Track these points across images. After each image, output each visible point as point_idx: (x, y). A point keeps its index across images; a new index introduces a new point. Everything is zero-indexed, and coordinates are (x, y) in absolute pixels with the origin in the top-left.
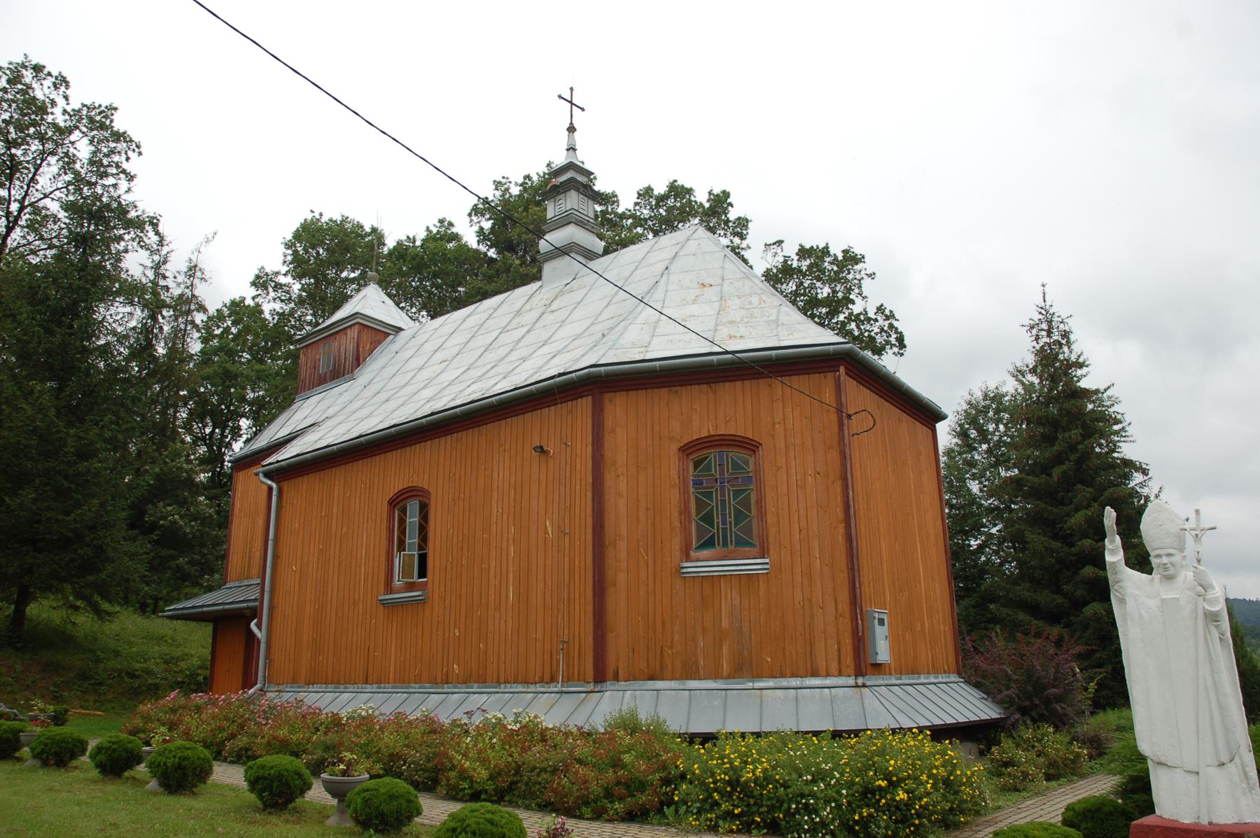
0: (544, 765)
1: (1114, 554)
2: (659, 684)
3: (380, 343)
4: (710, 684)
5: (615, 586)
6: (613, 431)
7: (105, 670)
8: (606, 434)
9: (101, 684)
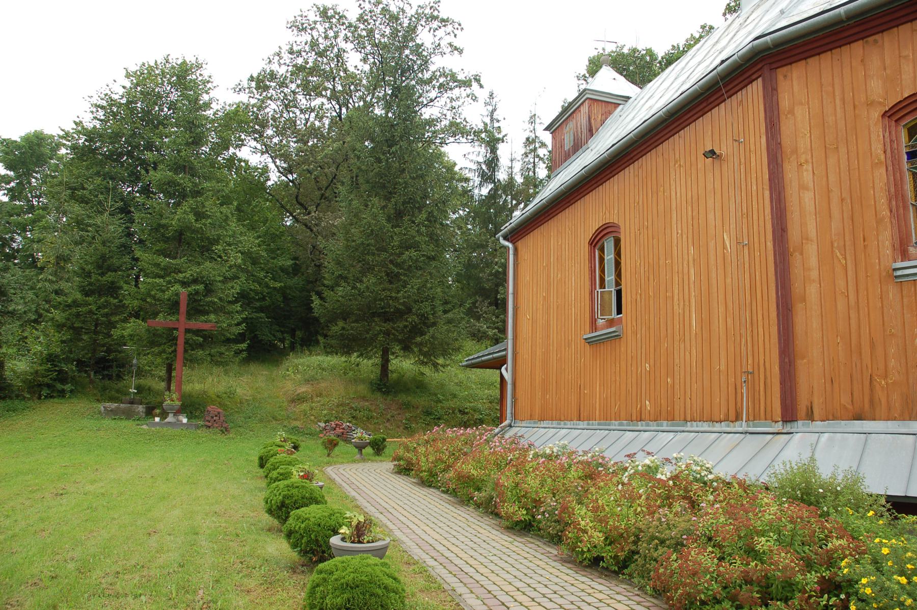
0: (666, 534)
2: (868, 425)
3: (610, 113)
4: (891, 426)
5: (804, 300)
6: (791, 112)
7: (442, 408)
8: (782, 117)
9: (439, 419)
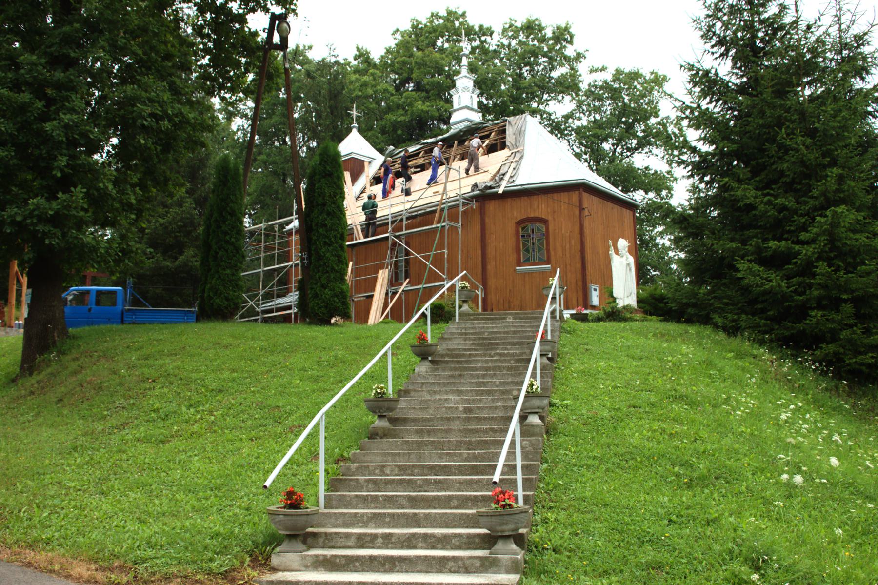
1: (612, 252)
